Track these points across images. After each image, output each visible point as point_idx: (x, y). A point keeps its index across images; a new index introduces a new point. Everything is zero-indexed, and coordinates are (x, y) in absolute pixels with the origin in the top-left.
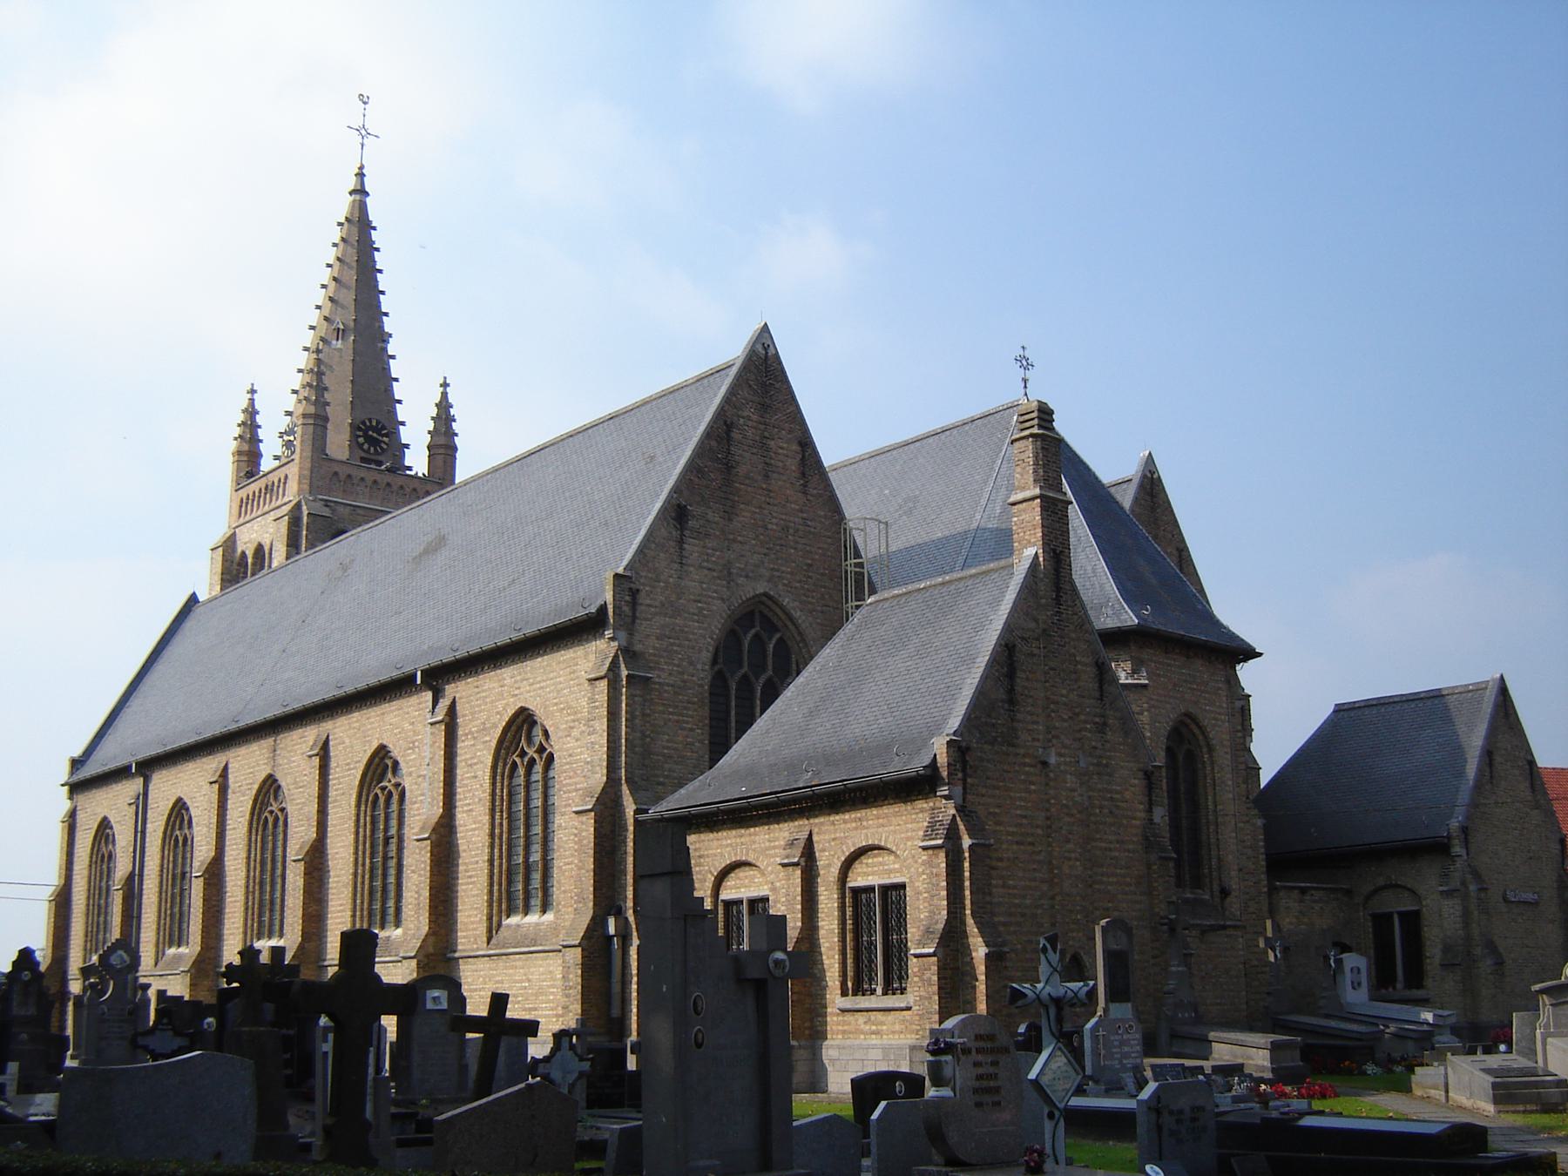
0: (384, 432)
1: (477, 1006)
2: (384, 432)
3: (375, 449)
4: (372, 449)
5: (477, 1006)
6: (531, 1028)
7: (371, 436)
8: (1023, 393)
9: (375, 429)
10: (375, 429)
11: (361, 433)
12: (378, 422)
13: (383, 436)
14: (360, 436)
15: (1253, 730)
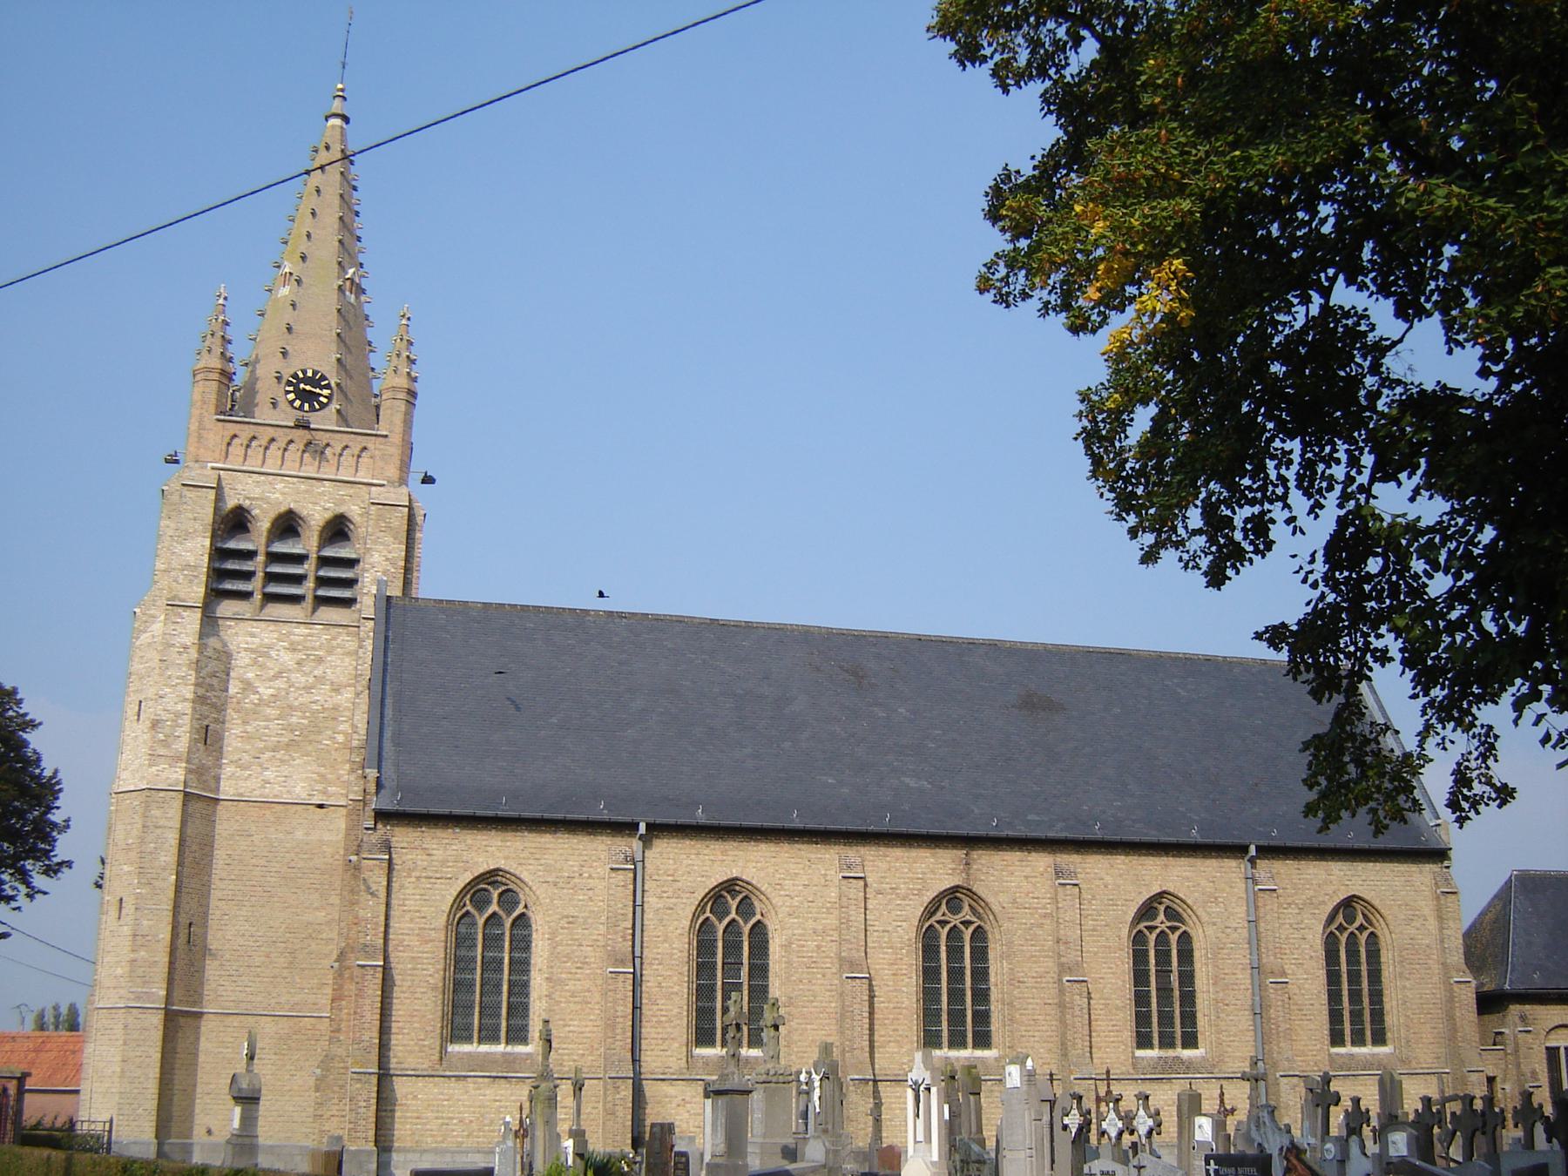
0: (323, 383)
1: (1400, 640)
2: (323, 383)
3: (311, 406)
4: (306, 406)
5: (1400, 640)
6: (1418, 559)
7: (304, 389)
8: (107, 866)
9: (306, 380)
10: (306, 380)
11: (291, 389)
12: (315, 373)
13: (322, 388)
14: (290, 392)
15: (1152, 419)
